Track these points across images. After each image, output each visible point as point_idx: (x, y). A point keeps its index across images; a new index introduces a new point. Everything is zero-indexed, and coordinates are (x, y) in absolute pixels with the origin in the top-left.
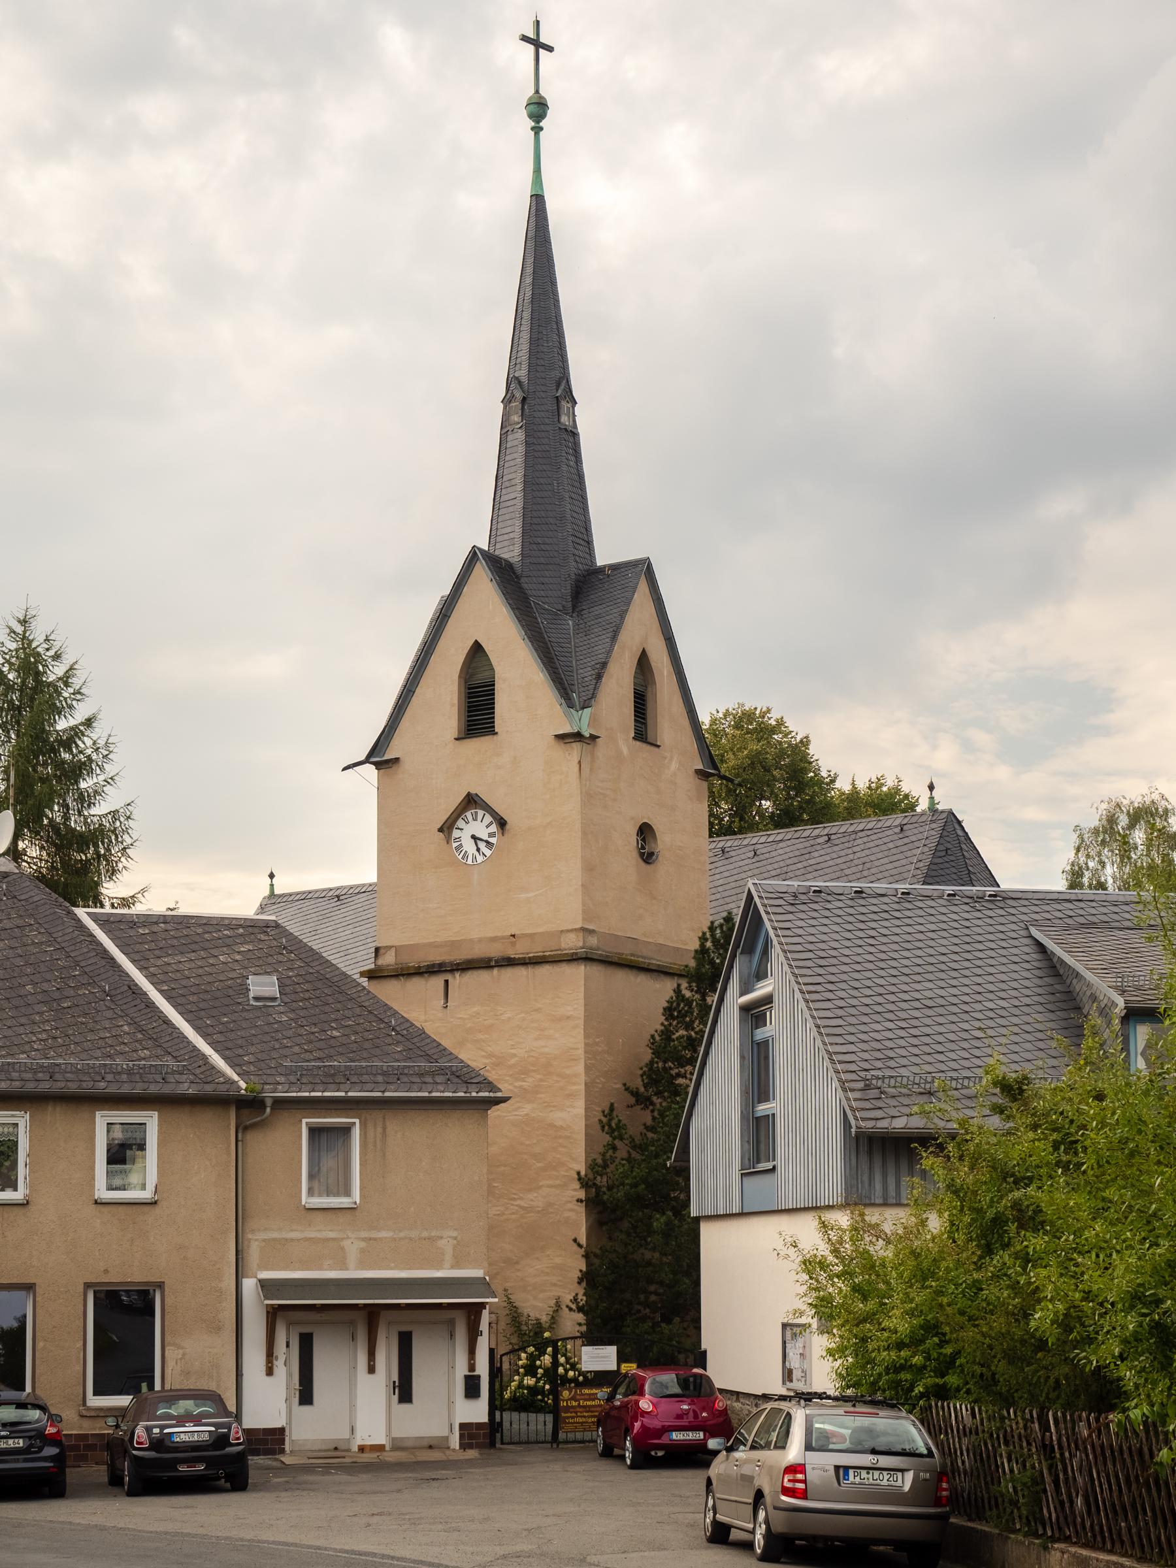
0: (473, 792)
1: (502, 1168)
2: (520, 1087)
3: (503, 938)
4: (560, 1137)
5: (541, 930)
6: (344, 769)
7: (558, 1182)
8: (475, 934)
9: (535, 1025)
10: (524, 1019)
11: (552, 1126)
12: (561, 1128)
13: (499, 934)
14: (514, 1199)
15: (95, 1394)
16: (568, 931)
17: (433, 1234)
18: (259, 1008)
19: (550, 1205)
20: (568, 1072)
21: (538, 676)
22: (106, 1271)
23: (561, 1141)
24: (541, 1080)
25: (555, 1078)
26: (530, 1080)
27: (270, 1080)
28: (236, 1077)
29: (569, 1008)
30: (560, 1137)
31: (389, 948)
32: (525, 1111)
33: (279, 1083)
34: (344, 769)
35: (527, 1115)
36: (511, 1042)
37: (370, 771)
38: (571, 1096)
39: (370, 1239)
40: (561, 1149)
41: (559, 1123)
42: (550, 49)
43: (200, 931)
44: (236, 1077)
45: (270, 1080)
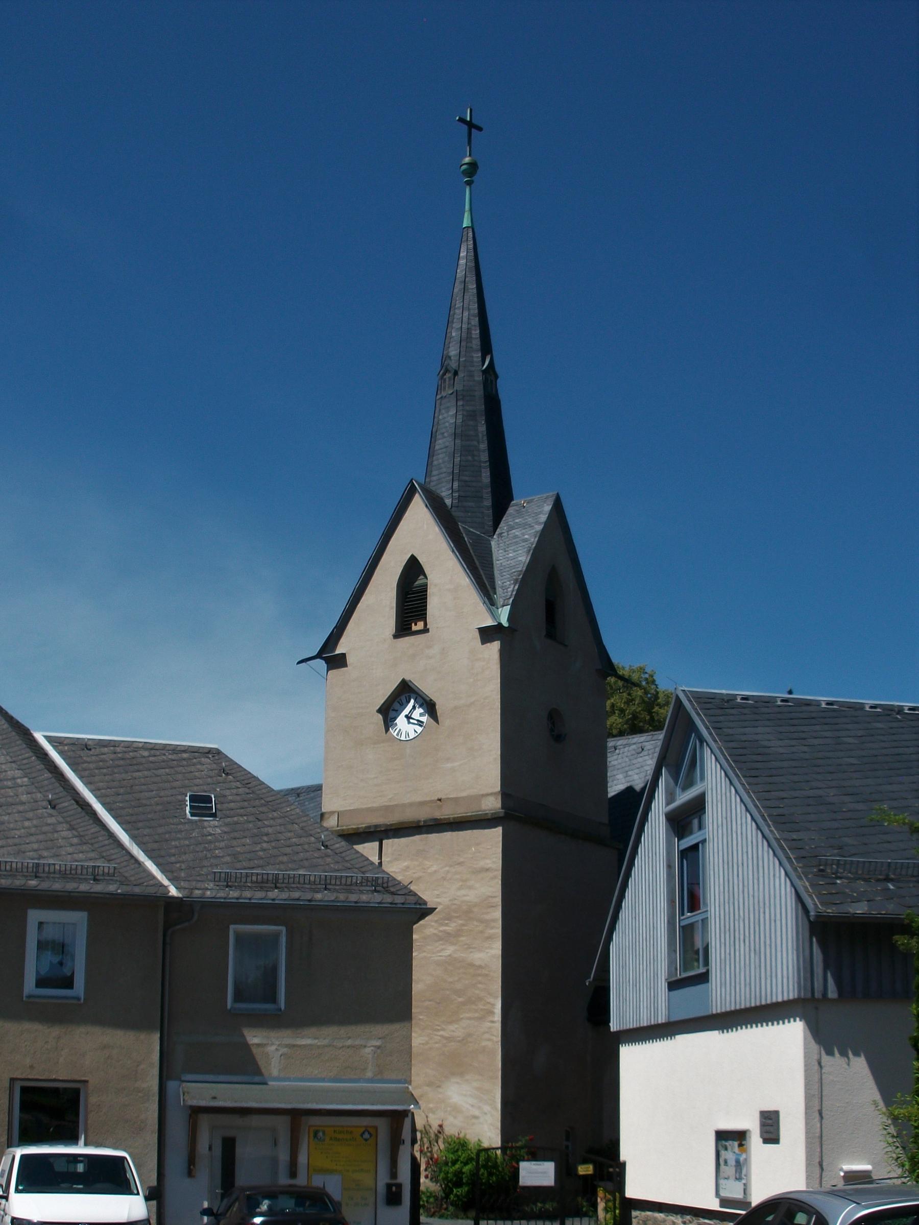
0: (407, 678)
1: (427, 1003)
2: (444, 931)
3: (432, 801)
4: (479, 975)
5: (464, 794)
6: (299, 663)
7: (476, 1015)
8: (407, 799)
9: (458, 876)
10: (448, 872)
11: (471, 965)
12: (480, 967)
13: (428, 799)
14: (438, 1030)
15: (17, 1191)
16: (488, 795)
17: (357, 1043)
18: (196, 821)
19: (470, 1035)
20: (487, 917)
21: (463, 580)
22: (32, 1067)
23: (480, 978)
24: (463, 925)
25: (475, 923)
26: (453, 925)
27: (199, 885)
28: (166, 882)
29: (488, 861)
30: (479, 975)
31: (332, 813)
32: (447, 953)
33: (207, 889)
34: (299, 663)
35: (450, 955)
36: (436, 892)
37: (321, 664)
38: (490, 938)
39: (294, 1046)
40: (480, 986)
41: (477, 963)
42: (480, 129)
43: (146, 754)
44: (166, 882)
45: (199, 885)
